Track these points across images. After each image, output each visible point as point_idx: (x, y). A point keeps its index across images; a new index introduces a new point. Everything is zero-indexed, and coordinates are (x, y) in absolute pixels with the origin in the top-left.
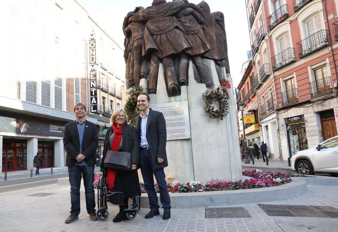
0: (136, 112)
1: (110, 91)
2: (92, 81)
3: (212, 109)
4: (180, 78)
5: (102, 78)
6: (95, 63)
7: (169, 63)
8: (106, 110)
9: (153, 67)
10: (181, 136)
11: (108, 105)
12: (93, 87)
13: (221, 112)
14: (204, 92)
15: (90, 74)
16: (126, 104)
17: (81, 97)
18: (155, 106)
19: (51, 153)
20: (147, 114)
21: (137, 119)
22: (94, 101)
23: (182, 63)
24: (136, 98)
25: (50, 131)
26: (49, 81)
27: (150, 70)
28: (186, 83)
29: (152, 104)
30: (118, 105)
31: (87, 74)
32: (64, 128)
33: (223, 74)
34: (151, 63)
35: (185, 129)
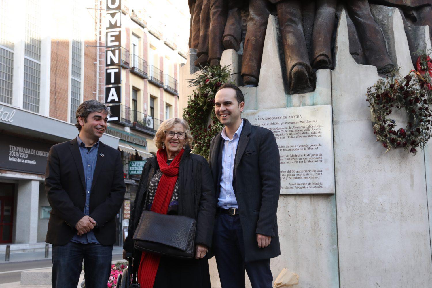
0: (210, 125)
1: (166, 84)
2: (112, 50)
3: (389, 125)
4: (316, 51)
5: (134, 45)
6: (119, 8)
7: (291, 14)
8: (141, 117)
9: (255, 24)
10: (312, 186)
11: (144, 106)
12: (112, 63)
13: (412, 133)
14: (372, 86)
15: (107, 33)
16: (188, 107)
17: (83, 87)
18: (253, 114)
19: (8, 211)
20: (238, 132)
21: (213, 142)
22: (113, 95)
23: (321, 16)
24: (211, 93)
25: (10, 159)
26: (11, 44)
27: (246, 30)
28: (329, 63)
29: (247, 109)
30: (167, 107)
31: (100, 34)
32: (47, 155)
33: (421, 44)
34: (248, 15)
35: (321, 171)
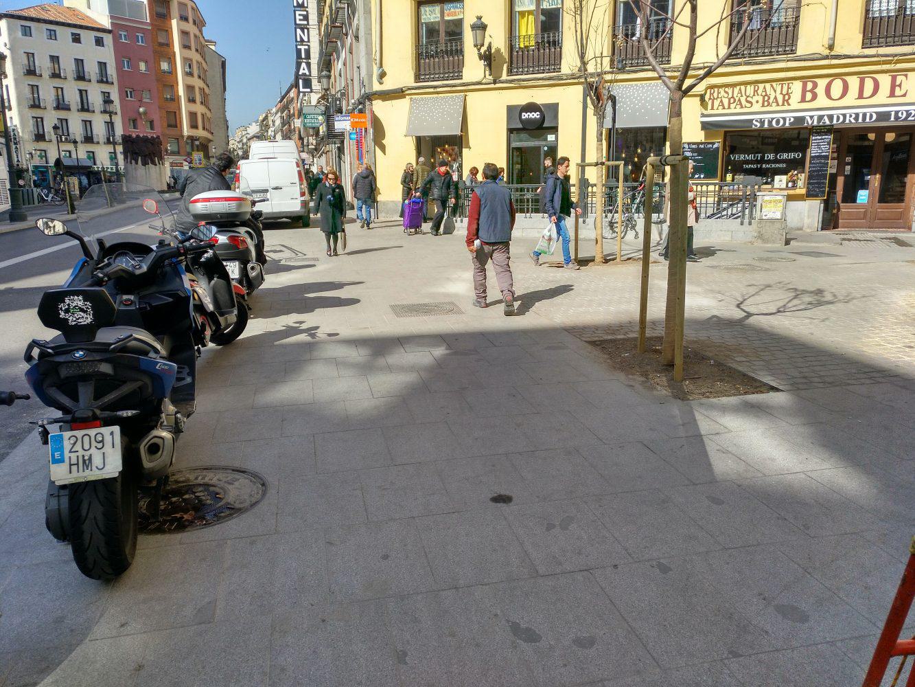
22: (304, 69)
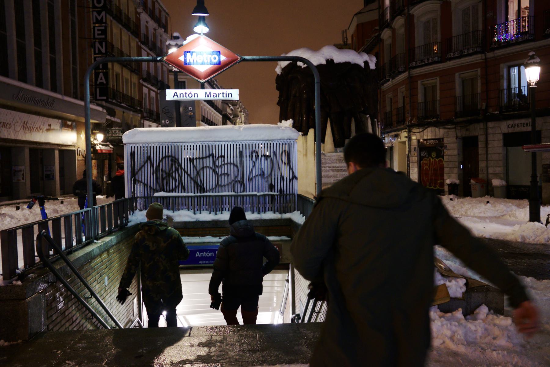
22: (101, 79)
